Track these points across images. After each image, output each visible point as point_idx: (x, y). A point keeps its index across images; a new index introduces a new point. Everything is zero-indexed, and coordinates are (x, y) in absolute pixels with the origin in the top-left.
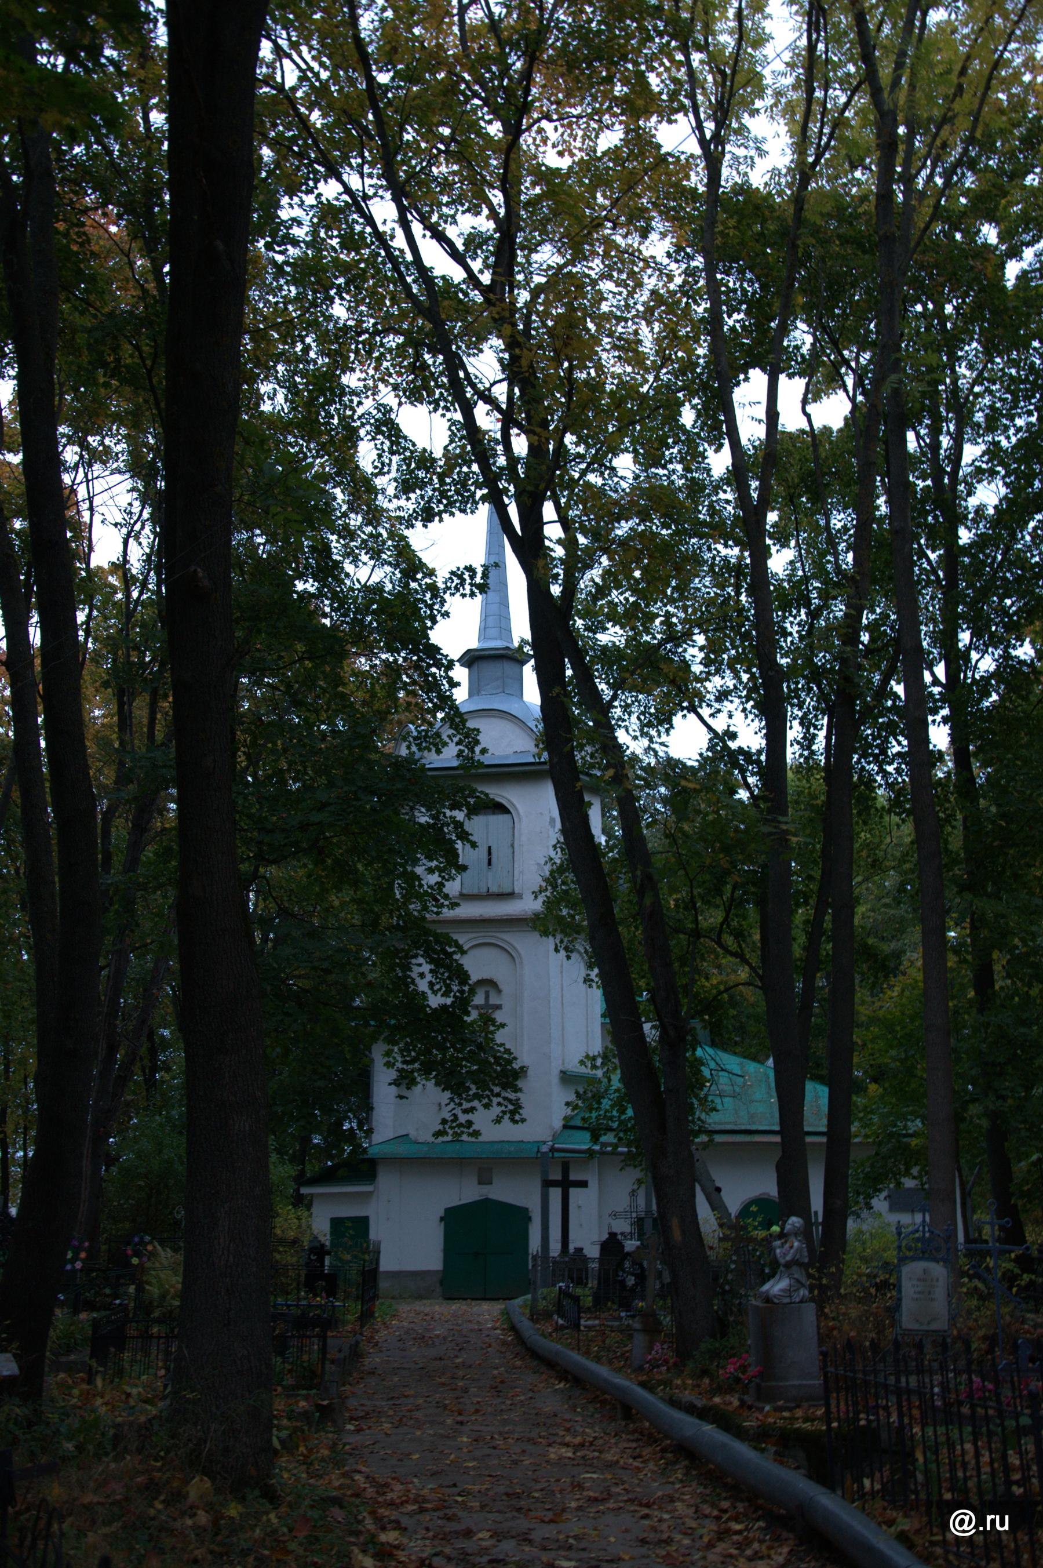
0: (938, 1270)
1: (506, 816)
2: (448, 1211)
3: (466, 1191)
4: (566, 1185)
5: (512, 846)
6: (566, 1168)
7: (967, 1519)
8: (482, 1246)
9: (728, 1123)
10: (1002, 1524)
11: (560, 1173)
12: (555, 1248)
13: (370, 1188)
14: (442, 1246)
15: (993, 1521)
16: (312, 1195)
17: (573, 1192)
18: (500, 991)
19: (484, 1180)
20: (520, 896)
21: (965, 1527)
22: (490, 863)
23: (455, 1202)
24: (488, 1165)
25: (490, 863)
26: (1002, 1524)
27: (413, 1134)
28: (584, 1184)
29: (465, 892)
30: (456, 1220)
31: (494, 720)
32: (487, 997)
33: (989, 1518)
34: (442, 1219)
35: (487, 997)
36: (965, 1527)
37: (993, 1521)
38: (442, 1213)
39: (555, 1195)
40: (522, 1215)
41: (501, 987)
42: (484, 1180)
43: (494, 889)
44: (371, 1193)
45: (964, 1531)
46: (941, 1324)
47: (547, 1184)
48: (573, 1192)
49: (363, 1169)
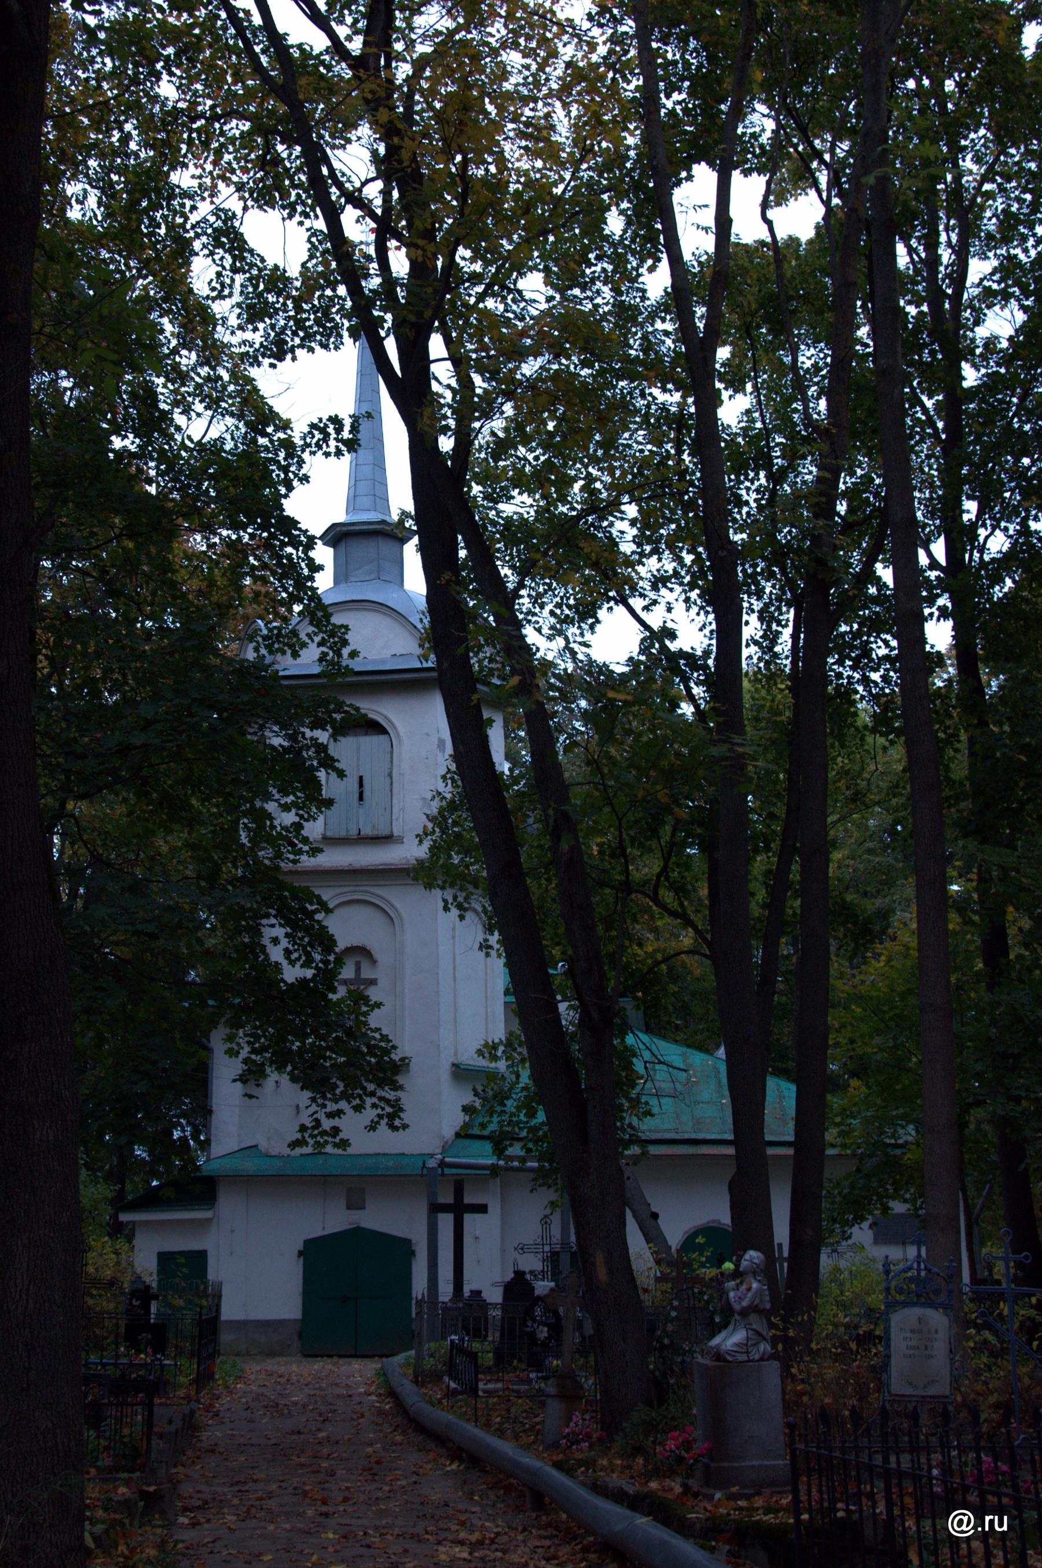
0: (937, 1319)
1: (382, 738)
2: (307, 1243)
3: (332, 1219)
4: (459, 1209)
5: (390, 776)
6: (459, 1189)
7: (965, 1519)
8: (353, 1289)
9: (668, 1131)
10: (1001, 1525)
11: (452, 1194)
12: (446, 1290)
13: (208, 1214)
14: (301, 1290)
15: (992, 1522)
16: (134, 1223)
17: (467, 1217)
18: (374, 962)
19: (355, 1204)
20: (400, 840)
21: (964, 1528)
22: (361, 798)
23: (317, 1230)
24: (358, 1184)
25: (361, 798)
26: (1001, 1525)
27: (263, 1144)
28: (482, 1209)
29: (329, 834)
30: (320, 1257)
31: (366, 614)
32: (358, 970)
33: (987, 1518)
34: (300, 1254)
35: (358, 970)
36: (964, 1528)
37: (992, 1522)
38: (300, 1246)
39: (446, 1222)
40: (403, 1249)
41: (377, 955)
42: (355, 1204)
43: (367, 831)
44: (208, 1221)
45: (962, 1532)
46: (941, 1388)
47: (435, 1209)
48: (467, 1217)
49: (199, 1189)
